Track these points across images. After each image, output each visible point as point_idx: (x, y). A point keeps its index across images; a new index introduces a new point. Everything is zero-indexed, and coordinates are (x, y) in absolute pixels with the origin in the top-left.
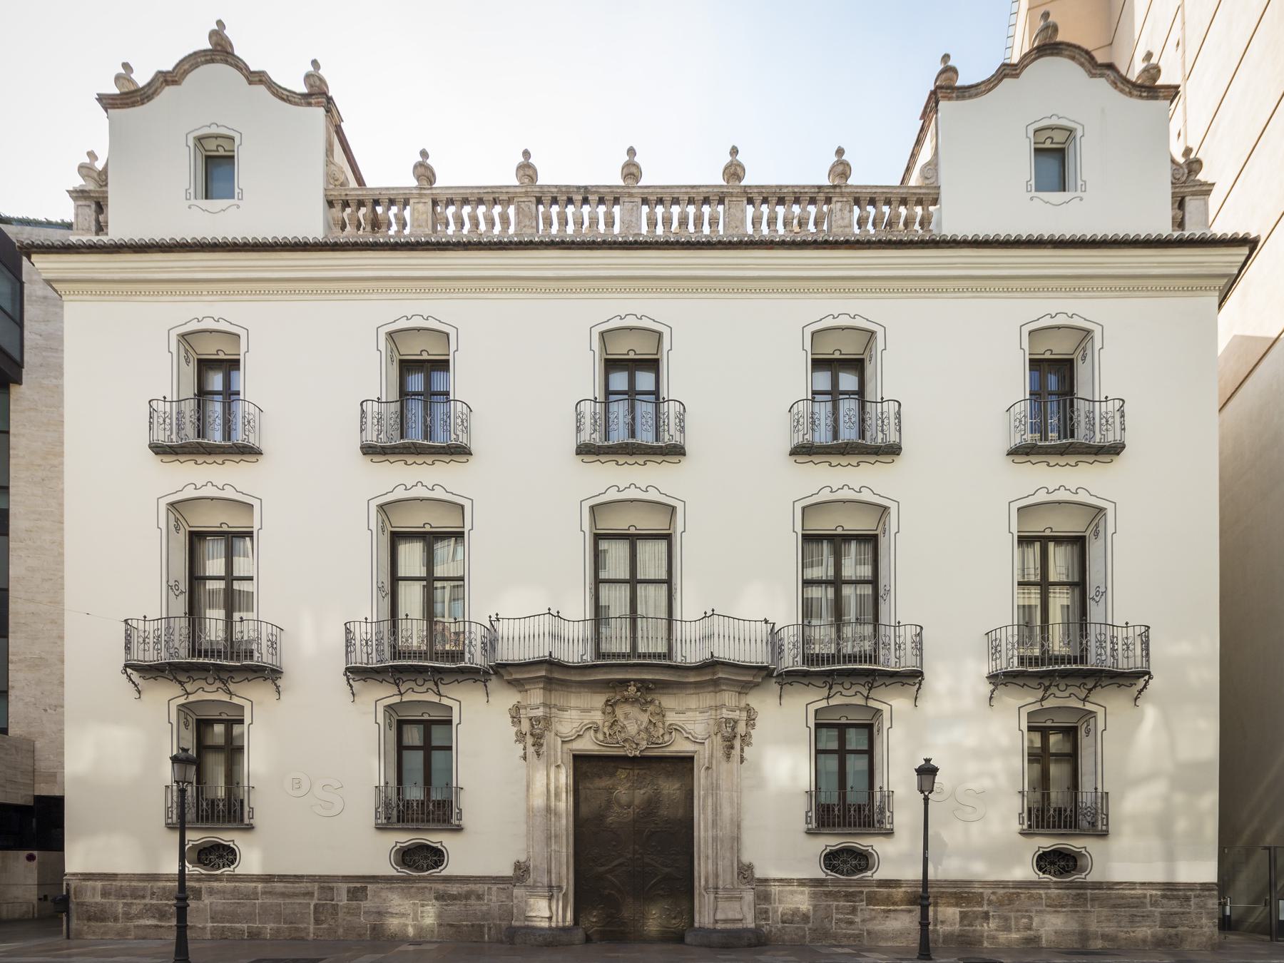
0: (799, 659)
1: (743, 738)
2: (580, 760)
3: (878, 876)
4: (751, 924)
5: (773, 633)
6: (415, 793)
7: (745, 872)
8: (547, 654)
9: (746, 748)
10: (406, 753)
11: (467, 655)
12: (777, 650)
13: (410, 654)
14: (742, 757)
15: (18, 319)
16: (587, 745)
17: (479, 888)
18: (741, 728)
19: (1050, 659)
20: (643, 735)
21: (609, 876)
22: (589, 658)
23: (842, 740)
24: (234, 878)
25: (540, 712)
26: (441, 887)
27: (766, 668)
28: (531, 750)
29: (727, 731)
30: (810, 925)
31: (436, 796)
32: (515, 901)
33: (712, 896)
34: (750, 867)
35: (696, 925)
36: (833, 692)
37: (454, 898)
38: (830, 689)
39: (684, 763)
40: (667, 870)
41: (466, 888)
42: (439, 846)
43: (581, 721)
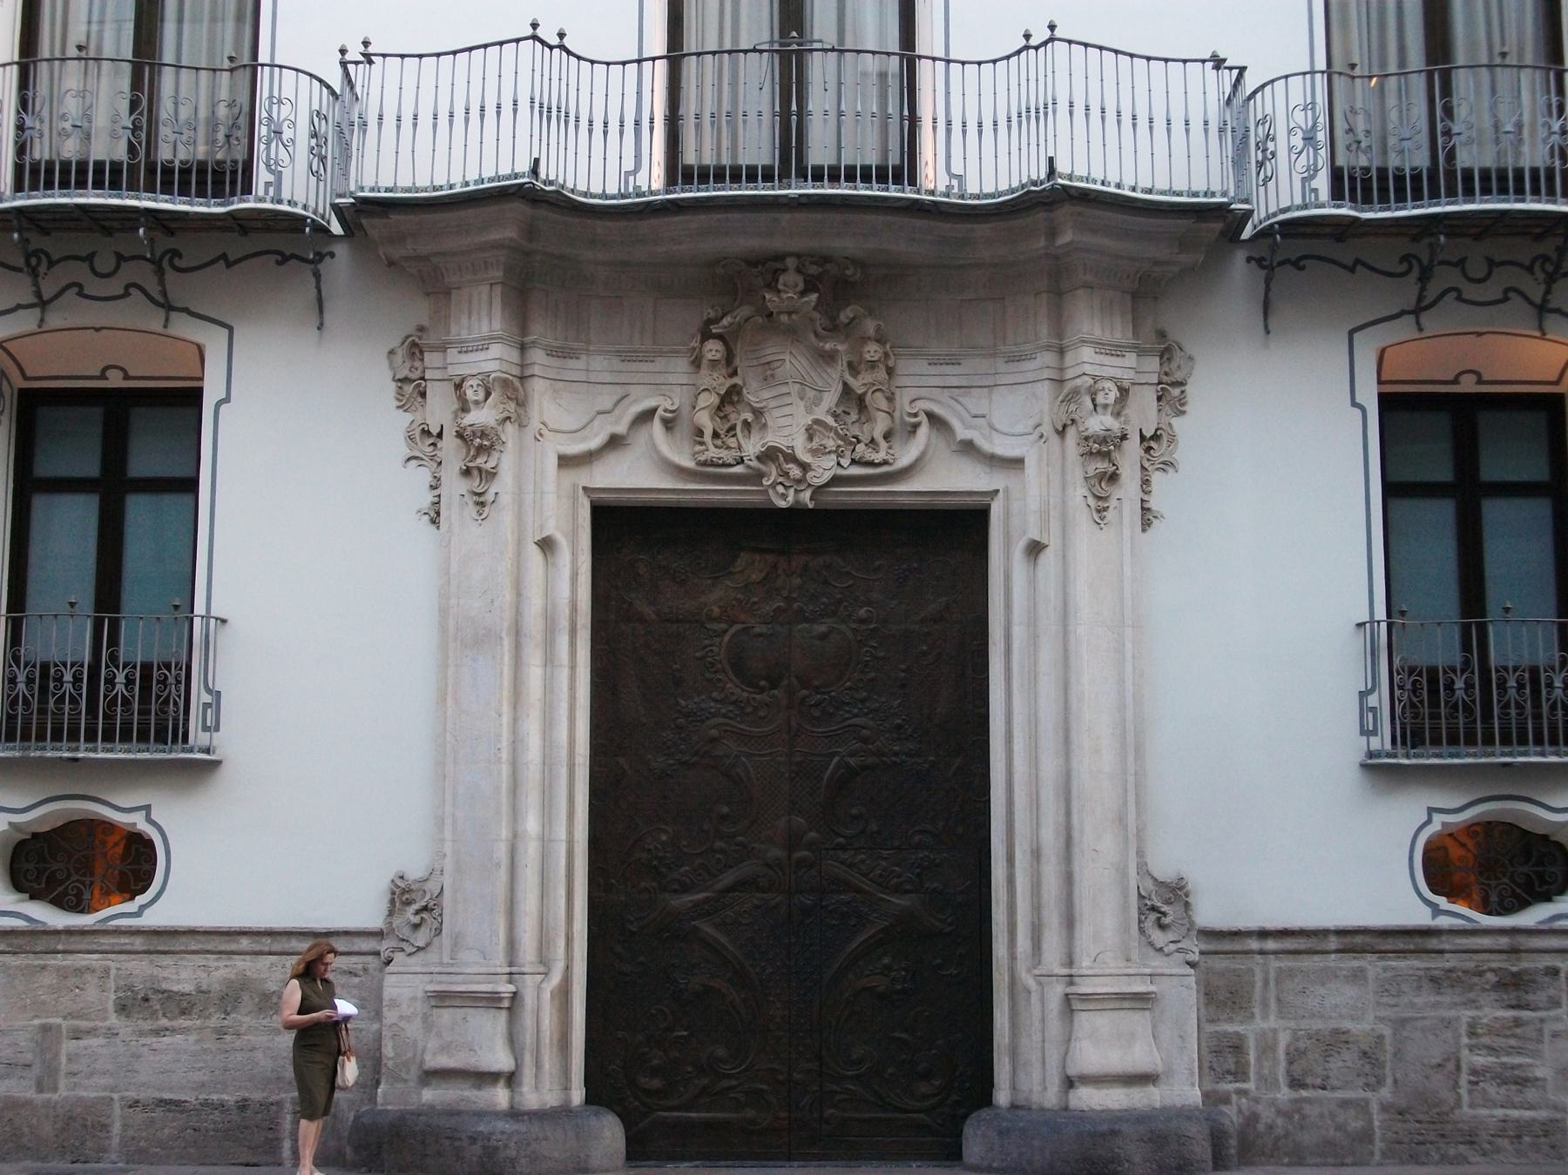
0: (1322, 182)
1: (1150, 441)
3: (152, 919)
4: (1185, 1091)
5: (1238, 95)
6: (65, 638)
7: (1163, 904)
8: (524, 166)
9: (1156, 478)
10: (39, 502)
11: (261, 176)
12: (1254, 155)
13: (75, 174)
14: (1145, 510)
15: (1426, 303)
21: (707, 928)
22: (653, 179)
23: (1466, 452)
24: (166, 939)
26: (140, 969)
27: (1221, 210)
28: (455, 487)
30: (1385, 1093)
31: (137, 644)
32: (390, 1016)
34: (1177, 892)
35: (1002, 1097)
36: (1432, 292)
37: (182, 1005)
38: (1424, 278)
39: (961, 530)
40: (901, 901)
41: (219, 972)
43: (604, 425)
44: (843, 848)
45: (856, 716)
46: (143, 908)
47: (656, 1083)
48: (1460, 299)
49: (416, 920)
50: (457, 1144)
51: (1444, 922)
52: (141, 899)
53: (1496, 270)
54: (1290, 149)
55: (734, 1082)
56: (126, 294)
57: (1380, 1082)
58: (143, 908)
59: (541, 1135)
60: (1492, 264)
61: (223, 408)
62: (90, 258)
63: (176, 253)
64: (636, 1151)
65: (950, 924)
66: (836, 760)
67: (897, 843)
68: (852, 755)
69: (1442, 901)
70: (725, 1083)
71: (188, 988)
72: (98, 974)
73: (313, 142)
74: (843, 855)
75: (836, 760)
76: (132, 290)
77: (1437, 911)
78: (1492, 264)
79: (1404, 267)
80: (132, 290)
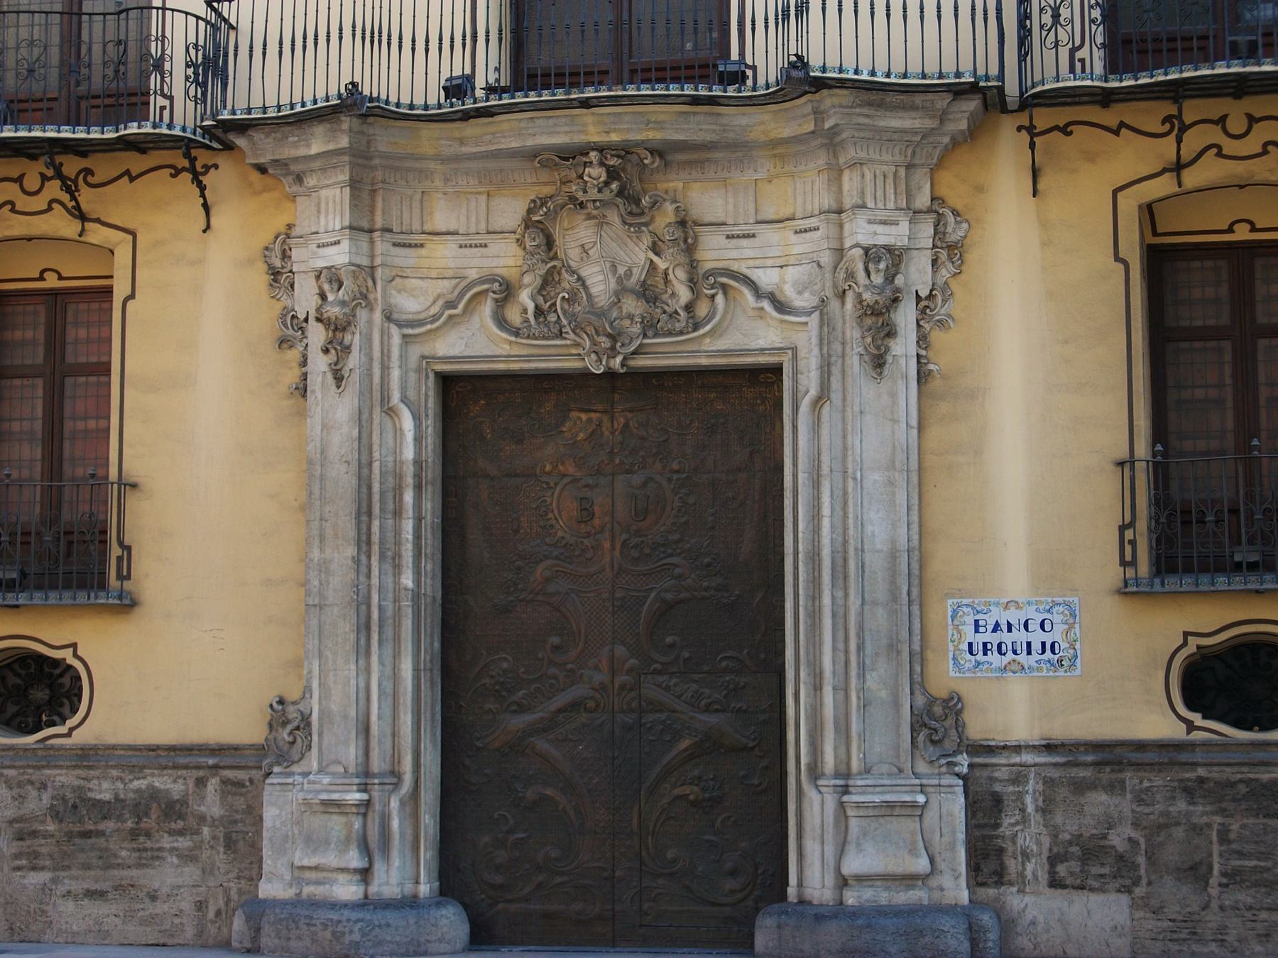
1: (925, 305)
2: (458, 392)
3: (83, 736)
9: (937, 336)
16: (478, 343)
17: (170, 784)
18: (918, 275)
19: (633, 72)
20: (631, 305)
21: (541, 744)
24: (88, 756)
25: (339, 256)
28: (320, 364)
29: (868, 286)
33: (831, 802)
34: (953, 706)
39: (761, 382)
40: (713, 719)
42: (67, 655)
44: (660, 673)
45: (671, 555)
46: (72, 729)
47: (498, 879)
48: (1220, 154)
49: (291, 739)
50: (313, 929)
51: (1198, 735)
52: (70, 723)
53: (1256, 127)
54: (1042, 27)
55: (565, 878)
56: (50, 209)
57: (1136, 882)
58: (72, 729)
59: (383, 922)
60: (1252, 120)
61: (130, 304)
62: (19, 180)
63: (89, 172)
64: (480, 935)
65: (754, 740)
66: (653, 595)
67: (706, 668)
68: (666, 591)
69: (1197, 718)
70: (559, 879)
71: (107, 796)
72: (37, 785)
73: (190, 71)
74: (660, 679)
75: (653, 595)
76: (54, 205)
77: (1191, 727)
78: (1252, 120)
79: (1167, 126)
80: (54, 205)
